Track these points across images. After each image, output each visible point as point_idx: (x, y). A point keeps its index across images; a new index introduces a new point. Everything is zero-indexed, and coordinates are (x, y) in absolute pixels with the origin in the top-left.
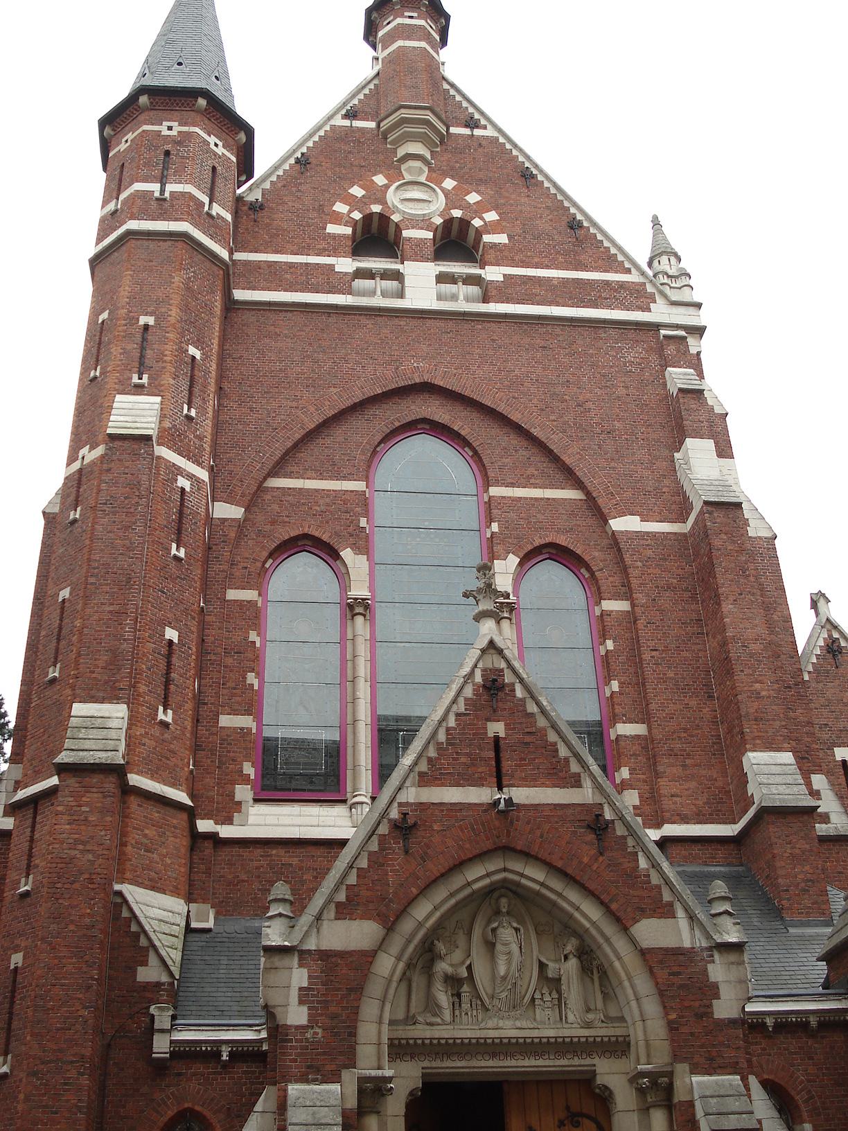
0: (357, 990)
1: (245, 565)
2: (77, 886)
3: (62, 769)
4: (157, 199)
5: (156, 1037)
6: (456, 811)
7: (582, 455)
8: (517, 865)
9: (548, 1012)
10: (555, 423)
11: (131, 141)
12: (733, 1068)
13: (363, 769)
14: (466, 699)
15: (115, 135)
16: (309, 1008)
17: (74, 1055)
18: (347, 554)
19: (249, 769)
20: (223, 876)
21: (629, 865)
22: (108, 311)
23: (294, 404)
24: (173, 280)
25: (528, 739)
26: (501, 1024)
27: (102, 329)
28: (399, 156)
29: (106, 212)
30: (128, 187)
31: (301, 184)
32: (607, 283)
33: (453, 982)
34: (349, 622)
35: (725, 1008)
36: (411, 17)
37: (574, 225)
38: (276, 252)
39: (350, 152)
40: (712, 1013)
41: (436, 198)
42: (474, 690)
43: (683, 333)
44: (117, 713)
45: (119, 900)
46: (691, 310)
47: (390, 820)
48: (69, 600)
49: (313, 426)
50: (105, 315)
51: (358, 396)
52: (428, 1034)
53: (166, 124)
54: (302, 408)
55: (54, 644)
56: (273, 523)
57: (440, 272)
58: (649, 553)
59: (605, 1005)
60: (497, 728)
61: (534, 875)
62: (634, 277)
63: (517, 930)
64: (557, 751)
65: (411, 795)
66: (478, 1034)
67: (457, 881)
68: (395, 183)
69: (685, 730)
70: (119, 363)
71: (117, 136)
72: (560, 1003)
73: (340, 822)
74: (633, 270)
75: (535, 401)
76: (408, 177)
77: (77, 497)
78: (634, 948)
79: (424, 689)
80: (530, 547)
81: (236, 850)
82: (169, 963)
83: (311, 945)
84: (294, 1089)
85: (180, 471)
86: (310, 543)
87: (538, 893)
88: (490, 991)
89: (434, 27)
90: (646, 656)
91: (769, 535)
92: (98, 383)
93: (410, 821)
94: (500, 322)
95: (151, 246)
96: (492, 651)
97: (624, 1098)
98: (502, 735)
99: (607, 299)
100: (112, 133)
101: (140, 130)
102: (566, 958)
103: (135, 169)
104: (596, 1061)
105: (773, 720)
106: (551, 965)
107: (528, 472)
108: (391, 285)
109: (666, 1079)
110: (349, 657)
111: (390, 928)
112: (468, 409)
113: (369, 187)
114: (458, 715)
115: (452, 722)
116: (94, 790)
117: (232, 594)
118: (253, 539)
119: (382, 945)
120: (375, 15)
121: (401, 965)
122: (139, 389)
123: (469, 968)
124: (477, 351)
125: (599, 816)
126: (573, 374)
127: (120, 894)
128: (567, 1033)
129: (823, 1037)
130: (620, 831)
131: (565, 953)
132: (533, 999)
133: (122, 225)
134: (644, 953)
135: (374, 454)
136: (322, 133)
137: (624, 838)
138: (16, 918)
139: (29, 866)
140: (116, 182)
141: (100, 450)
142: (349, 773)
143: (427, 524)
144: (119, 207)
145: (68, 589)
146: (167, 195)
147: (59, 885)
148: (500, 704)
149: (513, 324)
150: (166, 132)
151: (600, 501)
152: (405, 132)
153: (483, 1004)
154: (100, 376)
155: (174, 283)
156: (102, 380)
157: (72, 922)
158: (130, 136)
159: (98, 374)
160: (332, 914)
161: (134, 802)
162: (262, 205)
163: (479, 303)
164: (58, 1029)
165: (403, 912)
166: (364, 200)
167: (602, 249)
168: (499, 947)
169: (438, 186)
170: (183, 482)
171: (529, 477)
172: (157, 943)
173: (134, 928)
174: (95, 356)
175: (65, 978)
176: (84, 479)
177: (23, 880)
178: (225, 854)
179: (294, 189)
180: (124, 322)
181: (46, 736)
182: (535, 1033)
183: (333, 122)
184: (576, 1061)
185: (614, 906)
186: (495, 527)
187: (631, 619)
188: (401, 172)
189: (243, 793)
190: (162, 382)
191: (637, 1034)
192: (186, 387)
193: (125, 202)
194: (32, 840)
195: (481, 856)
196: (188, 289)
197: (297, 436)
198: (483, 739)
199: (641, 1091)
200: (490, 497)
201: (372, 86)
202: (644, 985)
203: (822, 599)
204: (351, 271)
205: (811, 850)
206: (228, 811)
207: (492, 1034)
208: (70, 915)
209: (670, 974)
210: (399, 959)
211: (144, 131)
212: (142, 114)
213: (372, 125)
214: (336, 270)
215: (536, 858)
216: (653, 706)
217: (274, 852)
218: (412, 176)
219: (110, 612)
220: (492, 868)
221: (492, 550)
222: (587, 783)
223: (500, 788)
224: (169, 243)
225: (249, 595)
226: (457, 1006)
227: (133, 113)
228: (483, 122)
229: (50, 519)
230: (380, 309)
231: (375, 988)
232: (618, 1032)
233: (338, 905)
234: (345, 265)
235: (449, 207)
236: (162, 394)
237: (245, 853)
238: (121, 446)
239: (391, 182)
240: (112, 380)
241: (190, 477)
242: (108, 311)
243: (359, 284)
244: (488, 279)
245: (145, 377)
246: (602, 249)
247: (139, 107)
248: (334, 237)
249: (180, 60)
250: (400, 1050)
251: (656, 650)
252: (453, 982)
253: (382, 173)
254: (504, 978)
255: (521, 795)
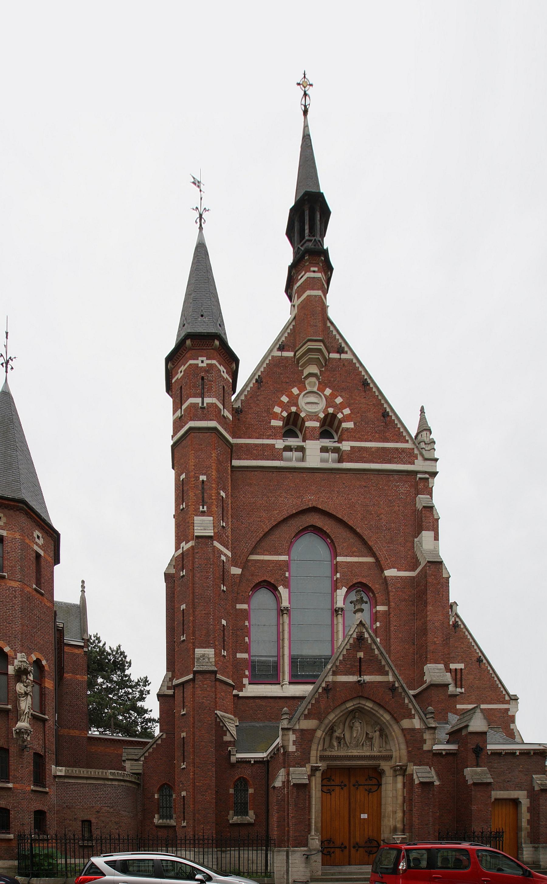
0: (311, 741)
1: (242, 594)
2: (206, 711)
3: (195, 673)
4: (201, 408)
5: (232, 756)
6: (345, 684)
7: (376, 541)
8: (363, 702)
9: (368, 748)
10: (367, 525)
11: (178, 373)
12: (427, 764)
13: (286, 672)
14: (350, 644)
15: (174, 367)
16: (296, 746)
17: (210, 762)
18: (281, 588)
19: (247, 673)
20: (240, 709)
21: (402, 702)
22: (184, 474)
23: (259, 519)
24: (212, 455)
25: (371, 658)
26: (353, 751)
27: (183, 483)
28: (305, 375)
29: (176, 417)
30: (186, 401)
31: (258, 395)
32: (397, 449)
33: (339, 739)
34: (281, 617)
35: (426, 747)
36: (314, 272)
37: (385, 415)
38: (249, 438)
39: (281, 374)
40: (423, 748)
41: (321, 401)
42: (353, 640)
43: (427, 476)
44: (210, 652)
45: (216, 716)
46: (432, 463)
47: (322, 687)
48: (185, 609)
49: (267, 530)
50: (183, 476)
51: (285, 514)
52: (330, 754)
53: (200, 358)
54: (263, 521)
55: (182, 627)
56: (252, 575)
57: (322, 446)
58: (399, 585)
59: (385, 745)
60: (361, 655)
61: (369, 705)
62: (409, 445)
63: (360, 723)
64: (381, 662)
65: (330, 678)
66: (346, 754)
67: (343, 707)
68: (303, 392)
69: (403, 657)
70: (194, 500)
71: (175, 368)
72: (372, 745)
73: (279, 691)
74: (409, 441)
75: (359, 515)
76: (309, 389)
77: (183, 565)
78: (399, 728)
79: (307, 643)
80: (351, 584)
81: (244, 700)
82: (234, 735)
83: (297, 727)
84: (291, 769)
85: (221, 553)
86: (266, 584)
87: (369, 711)
88: (349, 741)
89: (325, 279)
90: (392, 629)
91: (448, 576)
92: (185, 511)
93: (329, 687)
94: (347, 473)
95: (201, 436)
96: (361, 625)
97: (389, 772)
98: (362, 657)
99: (395, 458)
100: (173, 366)
101: (188, 364)
102: (375, 731)
103: (188, 389)
104: (381, 762)
105: (439, 652)
106: (370, 734)
107: (353, 550)
108: (300, 454)
109: (405, 767)
110: (281, 630)
111: (321, 722)
112: (331, 520)
113: (290, 395)
114: (347, 650)
115: (345, 652)
116: (208, 680)
117: (239, 606)
118: (245, 583)
119: (318, 727)
120: (294, 271)
121: (324, 733)
122: (203, 513)
123: (344, 735)
124: (336, 490)
125: (394, 685)
126: (377, 500)
127: (216, 714)
128: (373, 754)
129: (446, 758)
130: (400, 690)
131: (375, 730)
132: (363, 744)
133: (186, 424)
134: (403, 730)
135: (291, 544)
136: (267, 362)
137: (401, 693)
138: (181, 722)
139: (184, 705)
140: (179, 398)
141: (190, 544)
142: (281, 674)
143: (310, 575)
144: (183, 413)
145: (185, 605)
146: (205, 405)
147: (200, 711)
148: (362, 646)
149: (352, 474)
150: (201, 365)
151: (382, 562)
152: (309, 358)
153: (347, 745)
154: (186, 507)
155: (212, 457)
156: (187, 510)
157: (205, 722)
158: (183, 368)
159: (184, 506)
160: (303, 718)
161: (218, 683)
162: (241, 410)
163: (336, 463)
164: (204, 754)
165: (325, 717)
166: (288, 404)
167: (397, 429)
168: (354, 728)
169: (322, 393)
170: (223, 558)
171: (353, 552)
172: (229, 729)
173: (221, 724)
174: (181, 497)
175: (205, 740)
176: (184, 557)
177: (182, 710)
178: (241, 701)
179: (255, 399)
180: (193, 479)
181: (183, 661)
182: (363, 754)
183: (272, 354)
184: (374, 762)
185: (395, 715)
186: (338, 575)
187: (387, 614)
188: (305, 385)
189: (246, 681)
190: (212, 510)
191: (395, 754)
192: (221, 512)
193: (186, 410)
194: (183, 697)
195: (352, 699)
196: (218, 460)
197: (261, 535)
198: (356, 659)
199: (395, 771)
200: (337, 562)
201: (291, 327)
202: (401, 739)
203: (455, 604)
204: (283, 447)
205: (445, 699)
206: (241, 687)
207: (350, 754)
208: (204, 720)
209: (411, 736)
210: (323, 732)
211: (190, 364)
212: (188, 353)
213: (291, 354)
214: (276, 447)
215: (370, 699)
216: (392, 648)
217: (257, 701)
218: (310, 388)
219: (205, 613)
220: (355, 703)
221: (335, 586)
222: (390, 674)
223: (360, 676)
224: (208, 434)
225: (245, 606)
226: (339, 746)
227: (183, 352)
228: (346, 349)
229: (168, 577)
230: (295, 468)
231: (316, 741)
232: (390, 754)
233: (305, 715)
234: (280, 444)
235: (327, 407)
236: (213, 516)
237: (247, 701)
238: (201, 541)
239: (301, 391)
240: (192, 508)
241: (225, 555)
242: (184, 474)
243: (286, 454)
244: (344, 449)
245: (205, 507)
246: (397, 429)
247: (186, 348)
248: (274, 427)
249: (202, 313)
250: (322, 758)
251: (396, 626)
252: (339, 739)
253: (296, 386)
254: (355, 738)
255: (367, 678)
